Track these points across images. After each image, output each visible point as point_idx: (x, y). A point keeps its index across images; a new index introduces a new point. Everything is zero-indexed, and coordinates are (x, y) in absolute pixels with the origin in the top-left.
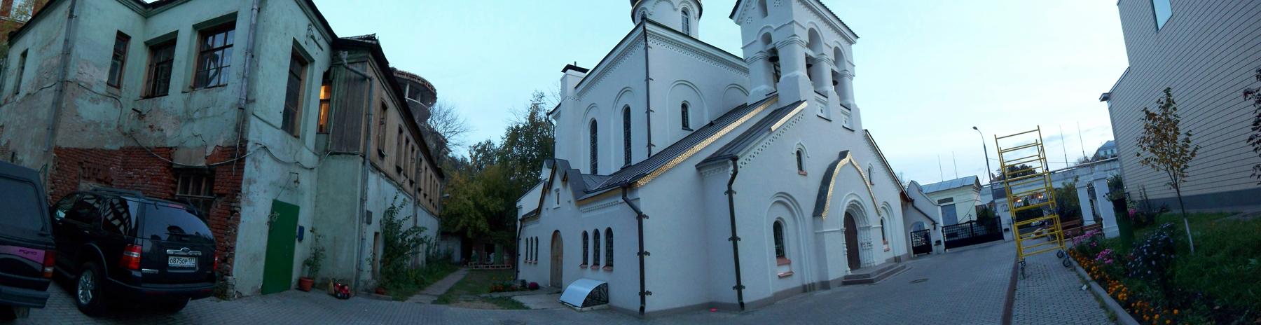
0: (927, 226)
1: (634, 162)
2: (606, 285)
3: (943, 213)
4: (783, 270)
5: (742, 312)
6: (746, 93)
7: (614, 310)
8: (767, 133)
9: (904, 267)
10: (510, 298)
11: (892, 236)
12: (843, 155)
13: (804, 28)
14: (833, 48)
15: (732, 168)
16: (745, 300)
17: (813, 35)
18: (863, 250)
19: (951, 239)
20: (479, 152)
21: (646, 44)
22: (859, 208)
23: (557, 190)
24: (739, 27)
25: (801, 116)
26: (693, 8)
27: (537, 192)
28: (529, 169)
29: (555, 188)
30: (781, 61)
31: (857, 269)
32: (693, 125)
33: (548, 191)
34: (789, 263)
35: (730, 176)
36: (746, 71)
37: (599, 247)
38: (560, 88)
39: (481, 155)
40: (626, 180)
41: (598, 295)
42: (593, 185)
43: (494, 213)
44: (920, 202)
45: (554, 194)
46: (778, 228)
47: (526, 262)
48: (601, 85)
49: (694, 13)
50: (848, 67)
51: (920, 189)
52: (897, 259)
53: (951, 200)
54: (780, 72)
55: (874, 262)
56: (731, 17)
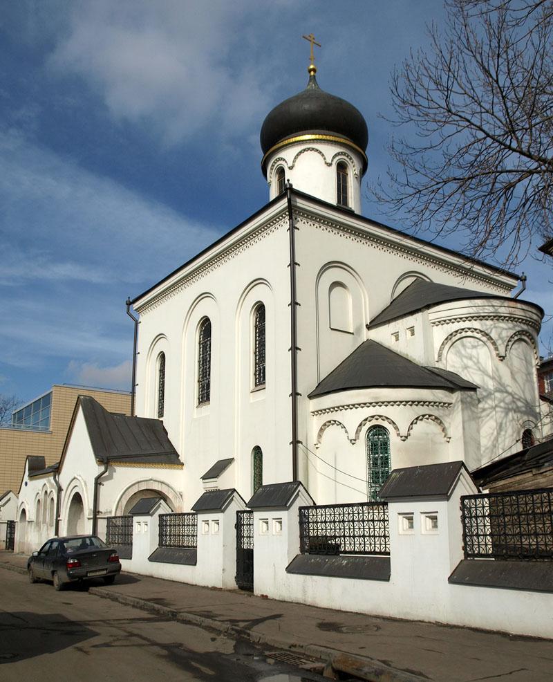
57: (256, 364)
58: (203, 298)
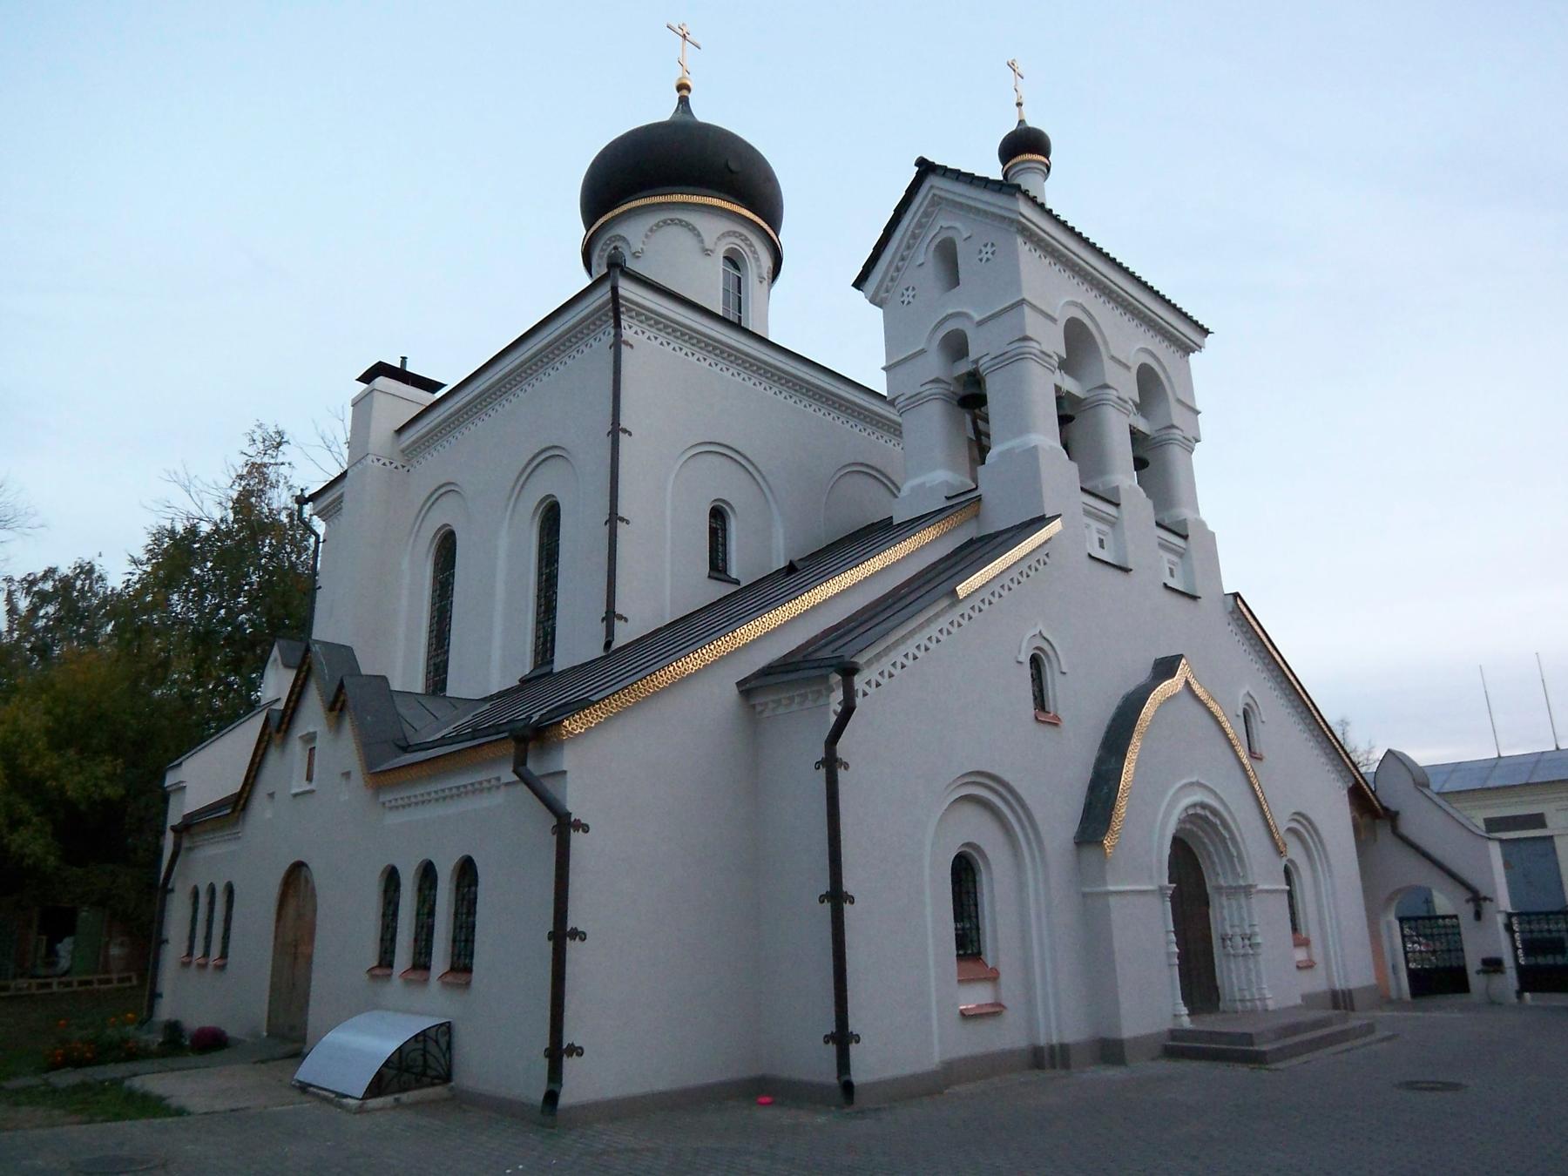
0: (1444, 902)
1: (561, 662)
2: (447, 1029)
3: (1507, 865)
4: (976, 996)
5: (847, 1110)
6: (893, 489)
7: (466, 1102)
8: (944, 603)
9: (1369, 1029)
10: (117, 1082)
11: (1321, 923)
12: (1166, 668)
13: (1053, 320)
14: (1134, 371)
15: (838, 695)
16: (858, 1076)
17: (1079, 339)
18: (1228, 955)
19: (1541, 960)
20: (44, 598)
21: (618, 335)
22: (1213, 826)
23: (310, 738)
24: (878, 313)
25: (1043, 558)
26: (755, 252)
27: (242, 739)
28: (224, 664)
29: (299, 735)
30: (994, 406)
31: (1210, 1012)
32: (740, 566)
33: (277, 738)
34: (993, 977)
35: (833, 718)
36: (895, 430)
37: (431, 913)
38: (349, 428)
39: (51, 609)
40: (530, 717)
41: (420, 1061)
42: (429, 727)
43: (83, 807)
44: (1421, 821)
45: (296, 748)
46: (965, 871)
47: (186, 965)
48: (477, 432)
49: (759, 267)
50: (1178, 416)
51: (1420, 778)
52: (1341, 1000)
53: (1538, 821)
54: (988, 436)
55: (1263, 999)
56: (858, 284)
57: (538, 622)
58: (437, 499)
